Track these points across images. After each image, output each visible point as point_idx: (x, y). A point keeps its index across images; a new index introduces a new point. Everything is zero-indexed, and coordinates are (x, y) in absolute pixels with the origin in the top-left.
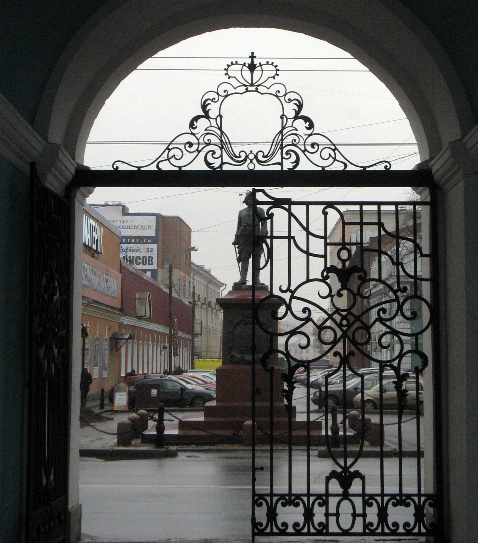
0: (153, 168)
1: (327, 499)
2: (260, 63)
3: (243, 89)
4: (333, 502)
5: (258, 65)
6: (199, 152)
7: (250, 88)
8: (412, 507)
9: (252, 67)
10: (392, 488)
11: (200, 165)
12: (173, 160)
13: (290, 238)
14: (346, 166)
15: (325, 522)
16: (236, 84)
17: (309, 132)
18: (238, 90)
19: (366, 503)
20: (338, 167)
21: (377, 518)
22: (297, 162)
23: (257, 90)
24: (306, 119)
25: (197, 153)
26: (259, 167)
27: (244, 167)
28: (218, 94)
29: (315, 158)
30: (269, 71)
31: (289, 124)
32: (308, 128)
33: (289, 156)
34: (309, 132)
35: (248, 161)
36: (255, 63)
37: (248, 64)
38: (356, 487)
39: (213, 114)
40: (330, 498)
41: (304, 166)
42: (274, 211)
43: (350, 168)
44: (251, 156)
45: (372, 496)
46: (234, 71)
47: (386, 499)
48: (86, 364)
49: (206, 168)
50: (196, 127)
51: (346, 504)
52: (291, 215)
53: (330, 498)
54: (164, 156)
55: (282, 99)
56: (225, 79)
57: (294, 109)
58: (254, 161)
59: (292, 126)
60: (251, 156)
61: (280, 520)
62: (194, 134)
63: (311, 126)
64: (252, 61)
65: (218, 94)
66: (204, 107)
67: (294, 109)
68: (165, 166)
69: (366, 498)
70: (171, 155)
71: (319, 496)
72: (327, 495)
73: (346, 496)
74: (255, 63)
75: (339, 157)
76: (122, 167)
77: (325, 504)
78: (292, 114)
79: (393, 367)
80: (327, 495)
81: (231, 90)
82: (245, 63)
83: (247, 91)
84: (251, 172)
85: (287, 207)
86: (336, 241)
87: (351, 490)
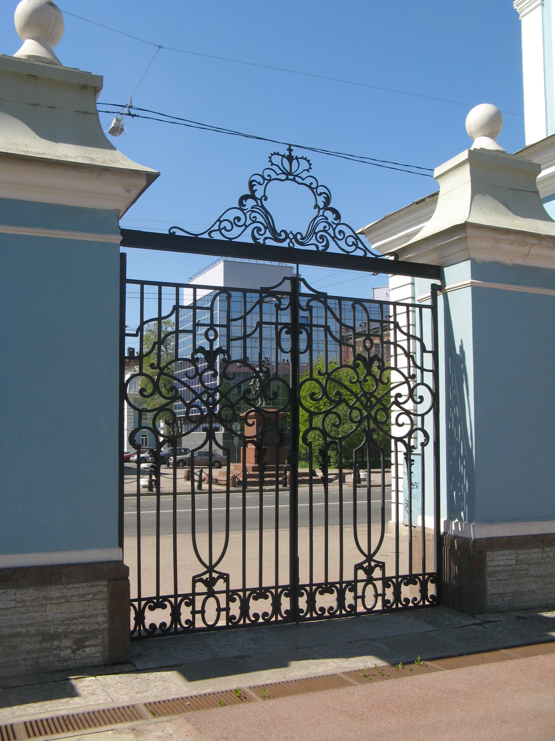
0: (206, 236)
1: (194, 598)
2: (296, 157)
3: (283, 177)
4: (199, 600)
5: (295, 157)
6: (247, 227)
7: (290, 177)
8: (270, 599)
9: (290, 158)
10: (252, 583)
11: (246, 238)
12: (223, 231)
13: (327, 329)
14: (366, 254)
15: (191, 620)
16: (279, 172)
17: (337, 222)
18: (279, 177)
19: (230, 599)
20: (360, 253)
21: (250, 605)
22: (327, 246)
23: (294, 180)
24: (334, 211)
25: (244, 227)
26: (297, 246)
27: (285, 244)
28: (318, 187)
29: (342, 244)
30: (304, 165)
31: (321, 214)
32: (336, 219)
33: (321, 241)
34: (337, 222)
35: (288, 240)
36: (292, 155)
37: (287, 155)
38: (377, 573)
39: (258, 194)
40: (197, 597)
41: (333, 249)
42: (313, 303)
43: (369, 255)
44: (291, 236)
45: (235, 592)
46: (277, 160)
47: (248, 593)
48: (139, 407)
49: (252, 242)
50: (245, 205)
51: (211, 602)
52: (327, 308)
53: (197, 597)
54: (216, 227)
55: (315, 190)
56: (269, 165)
57: (323, 201)
58: (293, 241)
59: (323, 215)
60: (291, 236)
61: (318, 606)
62: (242, 210)
63: (338, 217)
64: (290, 154)
65: (318, 187)
66: (251, 186)
67: (323, 201)
68: (217, 236)
69: (191, 597)
70: (222, 226)
71: (185, 596)
72: (194, 594)
73: (211, 593)
74: (292, 155)
75: (360, 245)
76: (179, 233)
77: (191, 603)
78: (321, 205)
79: (404, 443)
80: (194, 594)
81: (274, 176)
82: (285, 155)
83: (287, 179)
84: (290, 250)
85: (323, 299)
86: (250, 347)
87: (216, 588)
